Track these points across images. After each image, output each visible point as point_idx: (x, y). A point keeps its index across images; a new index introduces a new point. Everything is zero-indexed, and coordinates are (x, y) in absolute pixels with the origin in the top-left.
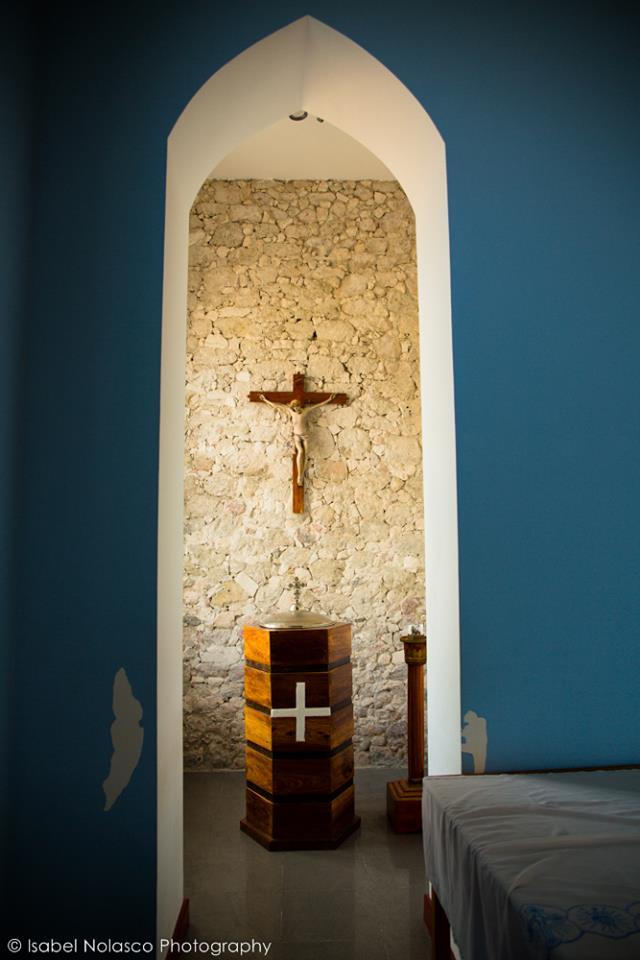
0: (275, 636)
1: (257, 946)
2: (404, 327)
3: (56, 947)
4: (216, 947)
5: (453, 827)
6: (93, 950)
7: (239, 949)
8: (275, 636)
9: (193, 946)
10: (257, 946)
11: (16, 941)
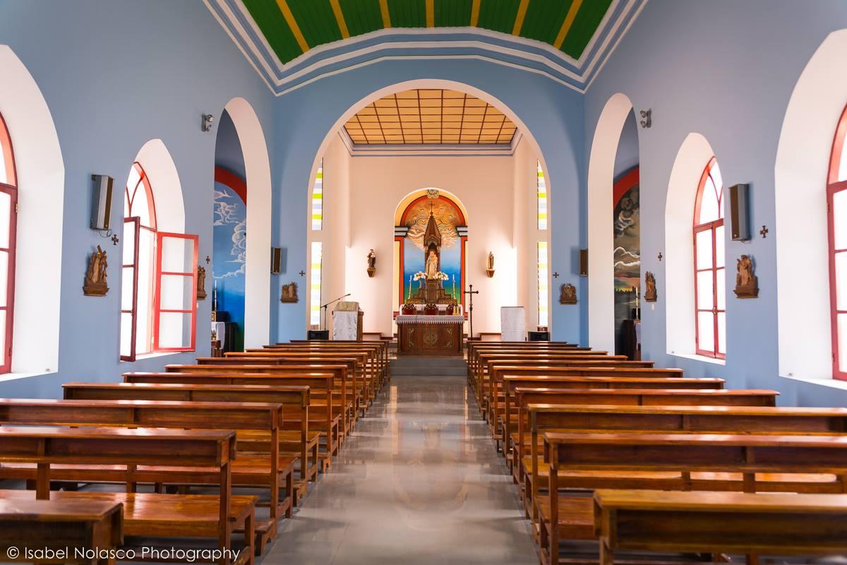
0: (577, 59)
1: (227, 553)
2: (632, 222)
3: (50, 554)
4: (191, 554)
5: (631, 311)
6: (83, 557)
7: (212, 553)
8: (577, 59)
9: (171, 553)
10: (227, 553)
11: (14, 549)
